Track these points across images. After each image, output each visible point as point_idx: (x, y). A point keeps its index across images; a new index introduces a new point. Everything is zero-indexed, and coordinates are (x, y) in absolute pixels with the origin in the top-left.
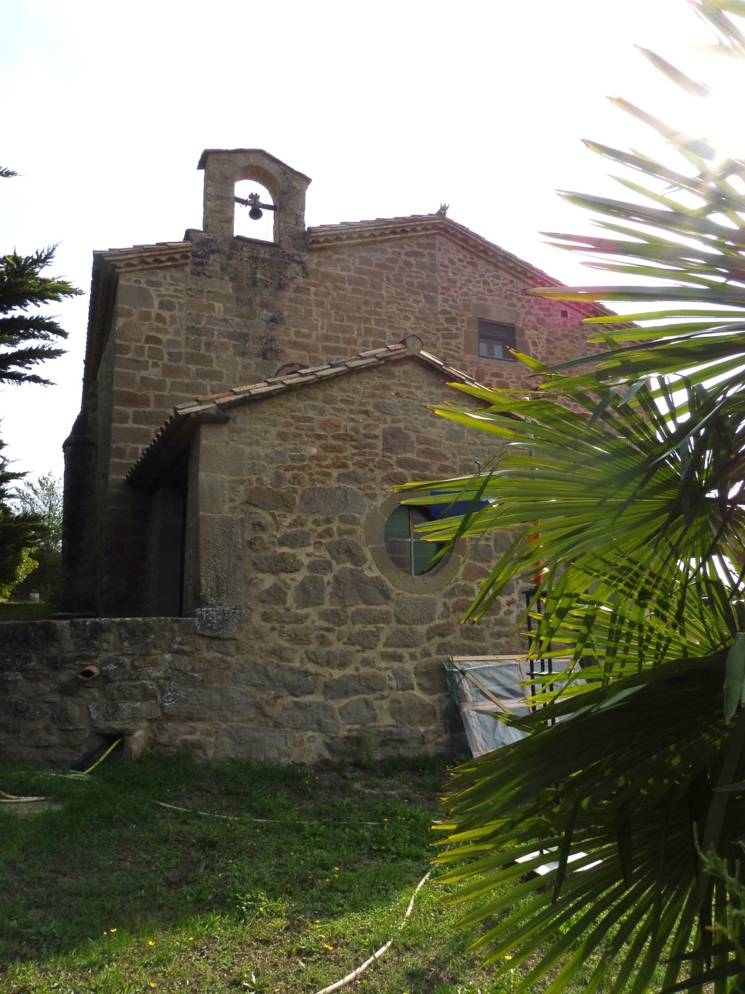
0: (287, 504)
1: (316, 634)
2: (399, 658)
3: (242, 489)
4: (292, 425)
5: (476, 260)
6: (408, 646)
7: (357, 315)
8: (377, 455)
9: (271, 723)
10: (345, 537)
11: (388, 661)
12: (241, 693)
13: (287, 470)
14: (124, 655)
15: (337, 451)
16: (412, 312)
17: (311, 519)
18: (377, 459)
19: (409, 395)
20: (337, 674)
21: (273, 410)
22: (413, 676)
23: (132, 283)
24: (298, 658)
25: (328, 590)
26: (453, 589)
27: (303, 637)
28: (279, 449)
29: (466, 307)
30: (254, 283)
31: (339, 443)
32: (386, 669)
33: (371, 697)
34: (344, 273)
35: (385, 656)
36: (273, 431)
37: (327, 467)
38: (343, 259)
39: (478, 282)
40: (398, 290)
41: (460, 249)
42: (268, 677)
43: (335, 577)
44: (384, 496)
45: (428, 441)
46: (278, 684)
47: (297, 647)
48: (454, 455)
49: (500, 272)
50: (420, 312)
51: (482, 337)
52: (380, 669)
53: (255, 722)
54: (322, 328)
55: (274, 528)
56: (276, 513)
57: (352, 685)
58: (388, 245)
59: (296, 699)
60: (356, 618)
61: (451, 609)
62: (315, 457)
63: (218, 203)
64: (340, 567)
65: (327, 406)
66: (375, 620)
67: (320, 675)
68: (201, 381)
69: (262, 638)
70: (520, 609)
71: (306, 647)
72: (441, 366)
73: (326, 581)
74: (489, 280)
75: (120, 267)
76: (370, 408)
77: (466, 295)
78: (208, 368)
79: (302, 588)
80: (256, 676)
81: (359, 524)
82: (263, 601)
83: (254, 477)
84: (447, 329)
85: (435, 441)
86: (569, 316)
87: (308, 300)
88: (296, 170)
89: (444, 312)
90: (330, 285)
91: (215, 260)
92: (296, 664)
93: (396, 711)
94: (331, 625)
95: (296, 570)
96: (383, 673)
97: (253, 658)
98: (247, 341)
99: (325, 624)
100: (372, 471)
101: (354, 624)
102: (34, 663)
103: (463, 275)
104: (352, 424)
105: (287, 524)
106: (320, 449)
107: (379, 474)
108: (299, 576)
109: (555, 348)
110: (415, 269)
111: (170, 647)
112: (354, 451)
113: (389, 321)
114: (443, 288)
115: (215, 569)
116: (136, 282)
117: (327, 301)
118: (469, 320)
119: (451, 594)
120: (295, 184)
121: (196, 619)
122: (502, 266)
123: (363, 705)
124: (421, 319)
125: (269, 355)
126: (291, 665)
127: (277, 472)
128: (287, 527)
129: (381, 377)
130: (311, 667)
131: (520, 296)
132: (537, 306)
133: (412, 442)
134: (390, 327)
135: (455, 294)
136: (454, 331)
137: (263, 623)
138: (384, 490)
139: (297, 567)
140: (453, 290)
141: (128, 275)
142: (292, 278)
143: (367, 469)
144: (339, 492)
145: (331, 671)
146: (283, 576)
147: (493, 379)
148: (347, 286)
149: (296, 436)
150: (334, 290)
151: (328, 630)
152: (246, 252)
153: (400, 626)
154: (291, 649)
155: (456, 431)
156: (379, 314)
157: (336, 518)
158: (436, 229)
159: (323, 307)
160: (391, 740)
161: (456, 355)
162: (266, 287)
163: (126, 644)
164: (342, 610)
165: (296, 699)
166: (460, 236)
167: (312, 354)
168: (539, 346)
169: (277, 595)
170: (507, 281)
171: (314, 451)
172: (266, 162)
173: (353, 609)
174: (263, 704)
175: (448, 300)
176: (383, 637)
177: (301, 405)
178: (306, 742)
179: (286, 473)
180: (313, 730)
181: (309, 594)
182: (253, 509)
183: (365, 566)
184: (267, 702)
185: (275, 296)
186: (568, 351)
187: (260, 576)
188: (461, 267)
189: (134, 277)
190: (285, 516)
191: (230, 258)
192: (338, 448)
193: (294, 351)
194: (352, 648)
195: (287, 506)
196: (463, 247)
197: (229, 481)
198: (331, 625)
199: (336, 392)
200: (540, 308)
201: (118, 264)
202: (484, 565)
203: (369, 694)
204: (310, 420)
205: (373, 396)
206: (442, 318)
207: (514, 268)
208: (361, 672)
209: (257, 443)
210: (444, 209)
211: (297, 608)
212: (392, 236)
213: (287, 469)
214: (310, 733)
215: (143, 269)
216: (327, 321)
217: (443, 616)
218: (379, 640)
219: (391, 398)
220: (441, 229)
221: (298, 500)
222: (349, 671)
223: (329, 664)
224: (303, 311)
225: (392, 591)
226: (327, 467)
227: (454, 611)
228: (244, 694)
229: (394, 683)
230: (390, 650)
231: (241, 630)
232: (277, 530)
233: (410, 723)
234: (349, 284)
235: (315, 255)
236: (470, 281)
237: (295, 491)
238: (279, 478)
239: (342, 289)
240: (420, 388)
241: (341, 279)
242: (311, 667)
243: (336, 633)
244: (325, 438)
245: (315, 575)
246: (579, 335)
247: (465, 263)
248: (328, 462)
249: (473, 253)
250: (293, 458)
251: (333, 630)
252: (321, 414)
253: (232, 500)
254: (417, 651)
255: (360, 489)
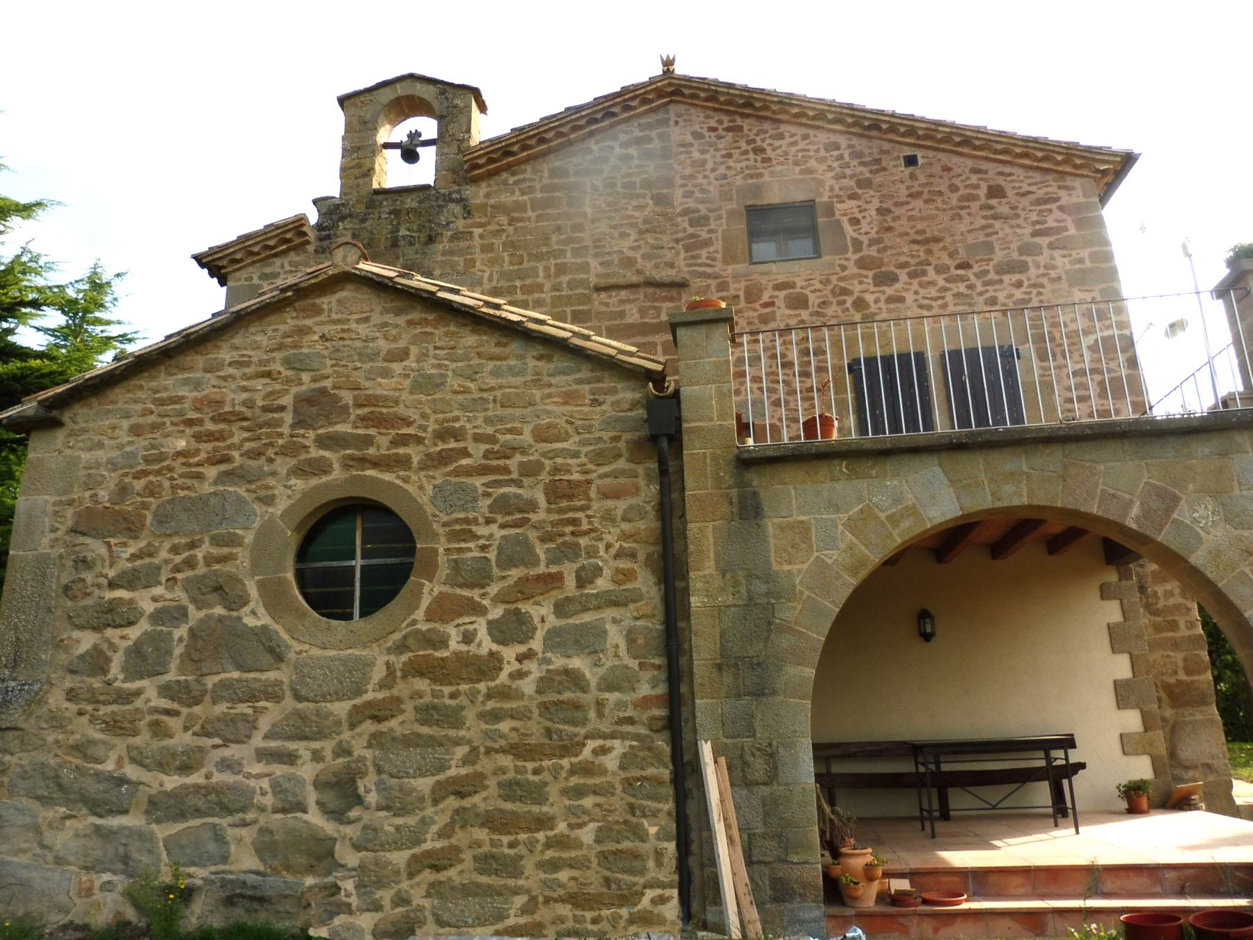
0: (131, 528)
1: (149, 718)
2: (290, 758)
3: (70, 512)
4: (152, 412)
5: (739, 121)
6: (306, 738)
7: (545, 249)
8: (281, 435)
9: (50, 858)
10: (216, 567)
11: (268, 763)
12: (16, 809)
13: (135, 478)
15: (217, 439)
16: (632, 225)
17: (167, 545)
18: (281, 442)
19: (344, 335)
20: (172, 782)
21: (130, 395)
22: (312, 788)
23: (243, 282)
24: (113, 756)
25: (178, 650)
26: (405, 637)
27: (126, 725)
28: (128, 449)
29: (726, 196)
30: (395, 244)
31: (222, 426)
32: (259, 776)
33: (224, 822)
34: (526, 198)
35: (264, 755)
36: (125, 424)
37: (198, 465)
38: (524, 180)
39: (746, 152)
40: (610, 199)
41: (711, 113)
42: (60, 786)
43: (191, 630)
44: (289, 497)
45: (373, 401)
46: (72, 797)
47: (117, 741)
48: (424, 416)
50: (645, 221)
51: (754, 235)
52: (249, 776)
53: (29, 854)
54: (490, 279)
55: (107, 563)
56: (113, 541)
57: (193, 801)
58: (592, 141)
59: (99, 821)
60: (227, 691)
61: (399, 674)
62: (179, 454)
63: (358, 155)
64: (202, 614)
65: (209, 375)
66: (251, 697)
67: (141, 783)
69: (61, 726)
70: (545, 667)
71: (131, 740)
72: (391, 279)
73: (176, 637)
74: (765, 145)
75: (223, 267)
76: (277, 367)
77: (725, 177)
79: (136, 651)
80: (43, 784)
81: (240, 545)
82: (73, 672)
83: (88, 494)
84: (692, 236)
85: (386, 398)
86: (920, 161)
87: (469, 247)
88: (456, 82)
89: (685, 212)
90: (504, 219)
91: (345, 229)
92: (109, 766)
93: (266, 847)
94: (176, 706)
95: (131, 624)
96: (252, 783)
97: (40, 757)
99: (165, 703)
100: (271, 461)
101: (214, 703)
103: (717, 150)
104: (245, 396)
105: (127, 555)
106: (192, 440)
107: (283, 465)
108: (134, 633)
109: (896, 219)
110: (636, 162)
112: (246, 435)
113: (595, 247)
114: (683, 178)
115: (16, 628)
116: (246, 279)
117: (498, 242)
118: (731, 214)
119: (401, 648)
120: (458, 102)
122: (781, 117)
123: (207, 834)
124: (648, 231)
126: (99, 767)
127: (120, 482)
128: (128, 560)
129: (297, 318)
130: (132, 772)
131: (823, 153)
132: (855, 162)
133: (346, 407)
134: (596, 255)
135: (705, 181)
136: (704, 235)
137: (67, 705)
138: (290, 487)
139: (132, 618)
140: (700, 176)
141: (237, 274)
142: (448, 224)
143: (263, 458)
144: (213, 501)
145: (165, 778)
146: (109, 632)
147: (776, 293)
148: (530, 213)
149: (155, 427)
150: (510, 224)
151: (168, 712)
152: (387, 206)
153: (300, 706)
154: (104, 743)
155: (430, 377)
156: (580, 240)
157: (207, 540)
158: (664, 97)
159: (492, 250)
160: (242, 896)
161: (709, 270)
162: (411, 244)
164: (198, 681)
165: (99, 821)
166: (703, 95)
168: (864, 224)
169: (97, 662)
170: (798, 138)
171: (181, 444)
172: (419, 86)
173: (216, 679)
174: (44, 827)
175: (693, 192)
176: (264, 724)
177: (169, 382)
178: (96, 890)
179: (135, 482)
180: (114, 873)
181: (143, 661)
182: (81, 539)
183: (246, 609)
184: (50, 826)
185: (424, 253)
186: (923, 219)
187: (76, 634)
188: (714, 139)
189: (243, 274)
190: (125, 544)
191: (364, 220)
192: (217, 435)
194: (208, 742)
195: (130, 530)
196: (715, 110)
197: (54, 504)
198: (176, 706)
199: (225, 353)
200: (862, 164)
201: (220, 263)
202: (475, 594)
203: (222, 817)
204: (179, 400)
205: (281, 347)
206: (683, 222)
208: (214, 780)
209: (100, 445)
210: (668, 63)
211: (123, 682)
212: (594, 127)
213: (137, 476)
214: (106, 877)
215: (254, 262)
216: (497, 268)
217: (382, 686)
218: (255, 728)
219: (311, 345)
220: (673, 93)
221: (149, 519)
222: (196, 778)
223: (162, 766)
224: (462, 263)
225: (287, 646)
226: (198, 465)
227: (404, 677)
228: (21, 811)
229: (269, 801)
230: (273, 744)
231: (30, 715)
232: (111, 567)
233: (288, 868)
234: (533, 210)
235: (484, 184)
236: (729, 156)
237: (145, 506)
238: (123, 490)
239: (521, 220)
240: (366, 320)
241: (520, 207)
242: (132, 772)
243: (183, 716)
244: (200, 422)
245: (159, 628)
246: (943, 188)
247: (720, 132)
248: (203, 456)
249: (735, 113)
250: (147, 460)
251: (176, 713)
252: (196, 389)
253: (54, 530)
254: (327, 746)
255: (248, 491)
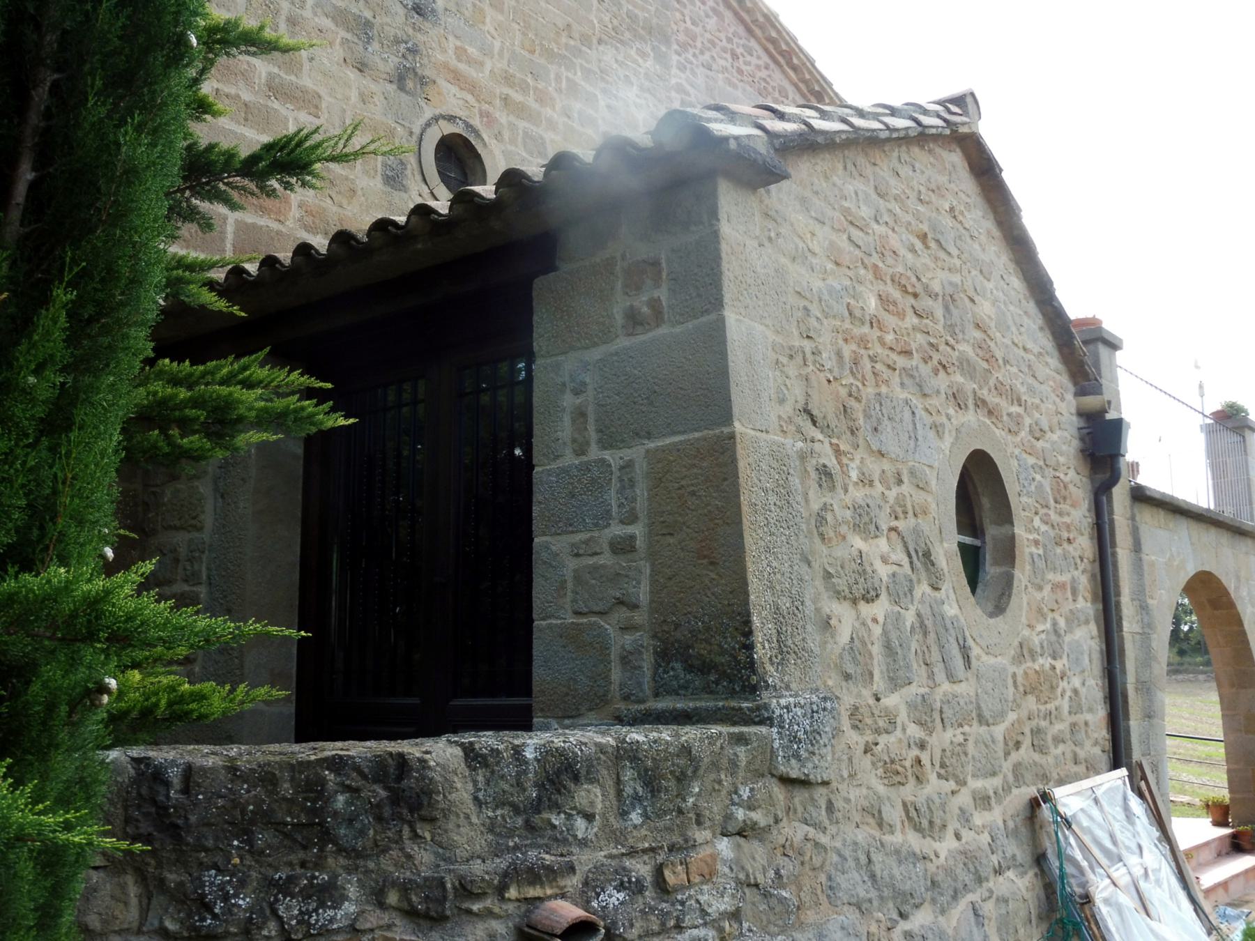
14: (633, 853)
49: (753, 43)
68: (276, 105)
78: (293, 78)
98: (369, 40)
102: (350, 908)
111: (728, 817)
121: (775, 730)
122: (758, 32)
125: (410, 84)
163: (635, 817)
167: (485, 107)
193: (454, 89)
207: (773, 41)
